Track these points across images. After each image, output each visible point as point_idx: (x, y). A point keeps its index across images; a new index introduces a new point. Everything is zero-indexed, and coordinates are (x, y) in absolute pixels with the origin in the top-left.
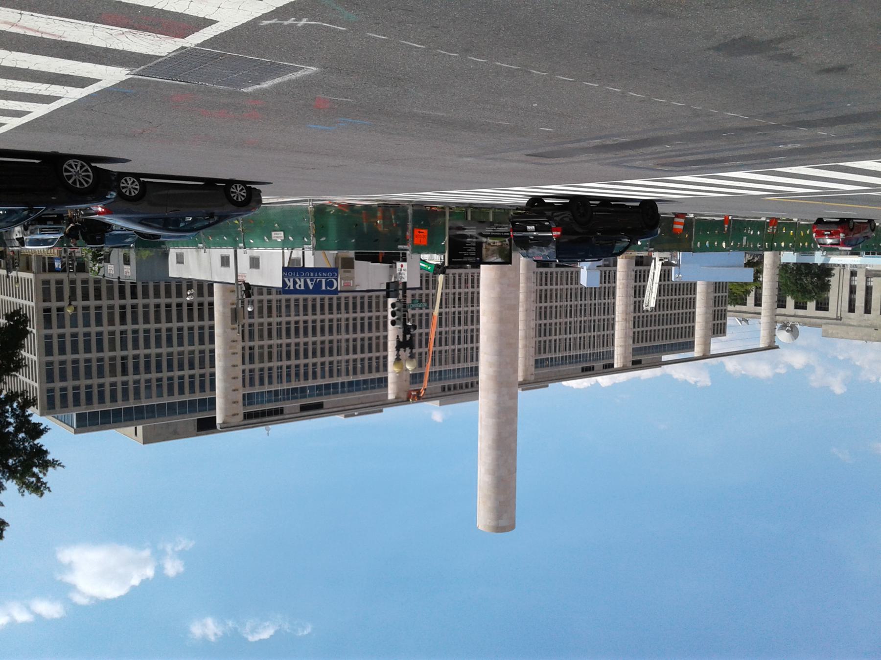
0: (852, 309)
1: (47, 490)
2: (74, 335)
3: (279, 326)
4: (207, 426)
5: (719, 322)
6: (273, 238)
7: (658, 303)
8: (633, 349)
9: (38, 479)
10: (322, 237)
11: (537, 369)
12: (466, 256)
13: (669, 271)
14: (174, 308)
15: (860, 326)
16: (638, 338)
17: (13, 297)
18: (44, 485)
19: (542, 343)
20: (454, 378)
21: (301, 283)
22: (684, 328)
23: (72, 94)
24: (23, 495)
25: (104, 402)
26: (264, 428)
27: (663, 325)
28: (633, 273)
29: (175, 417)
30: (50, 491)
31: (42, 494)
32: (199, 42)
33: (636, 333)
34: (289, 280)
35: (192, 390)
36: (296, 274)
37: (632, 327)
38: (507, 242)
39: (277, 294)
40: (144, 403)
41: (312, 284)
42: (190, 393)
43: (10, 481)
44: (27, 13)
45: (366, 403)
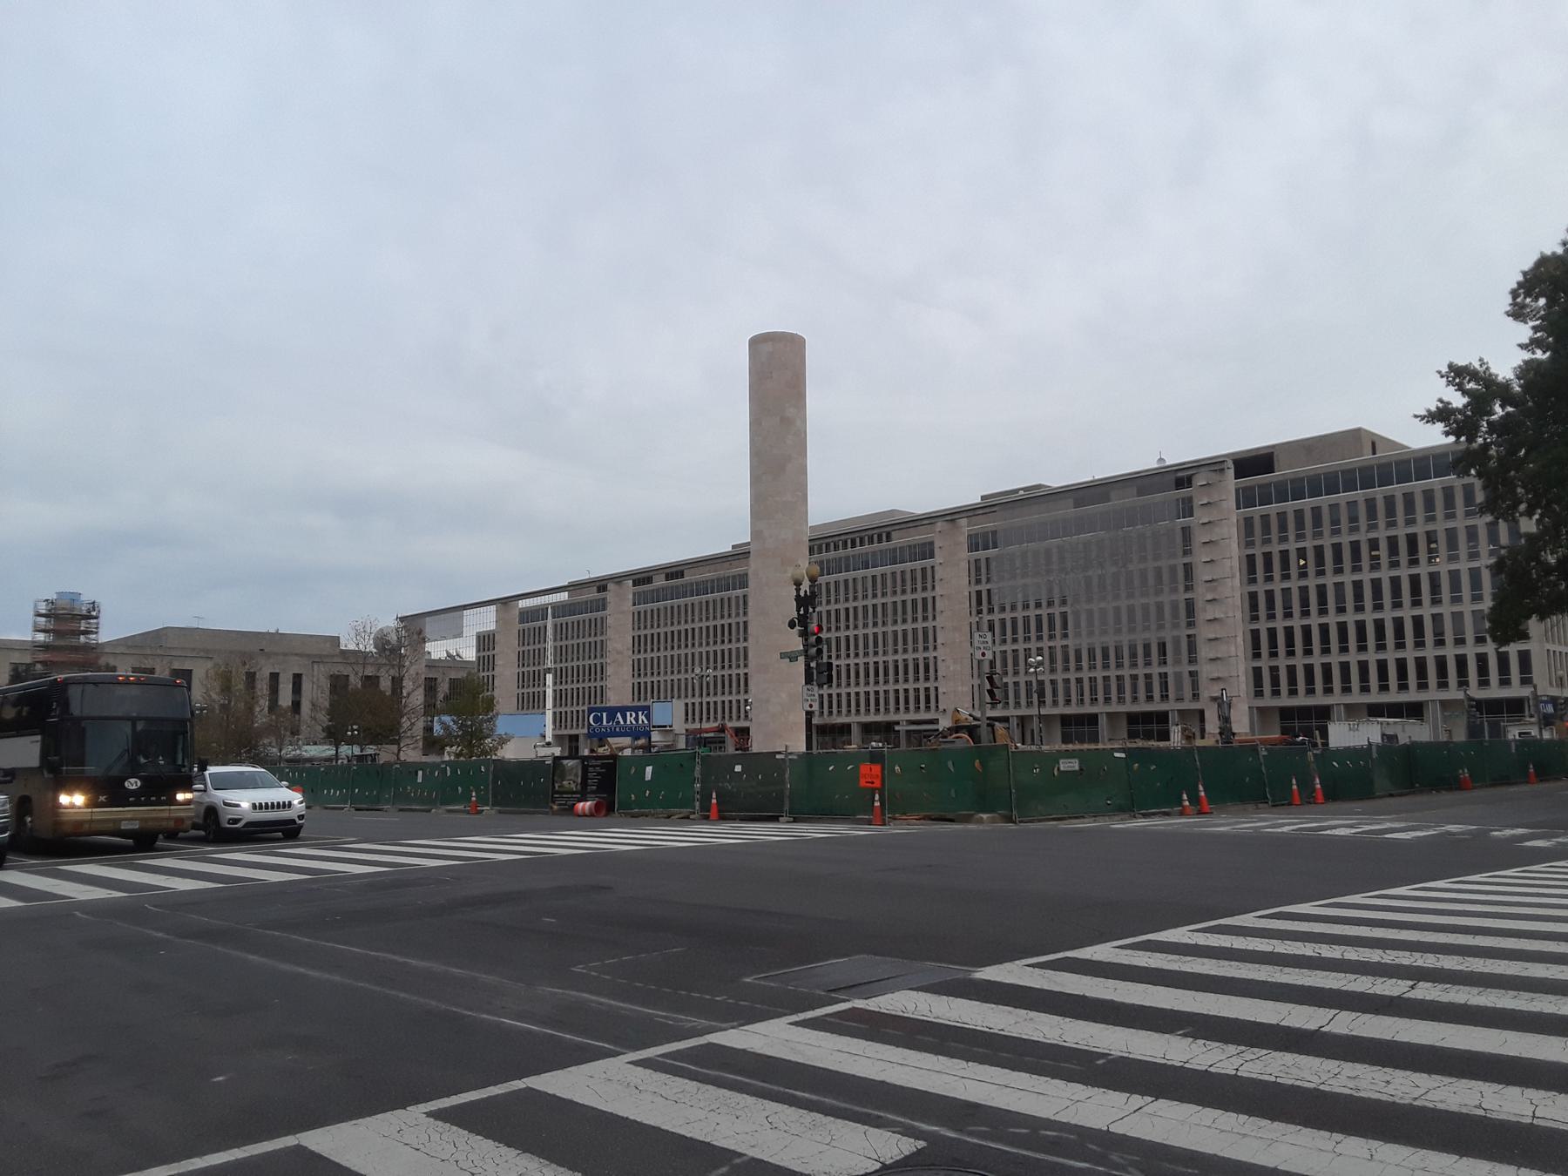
0: (297, 679)
3: (1027, 635)
4: (1253, 464)
5: (486, 653)
6: (1077, 761)
8: (932, 556)
9: (1460, 388)
13: (687, 719)
14: (1449, 637)
15: (285, 655)
16: (701, 610)
18: (1450, 379)
21: (630, 718)
24: (1481, 360)
26: (1168, 463)
29: (1293, 477)
30: (1439, 372)
31: (1451, 366)
34: (643, 722)
38: (557, 785)
40: (1359, 495)
42: (1412, 493)
45: (983, 514)
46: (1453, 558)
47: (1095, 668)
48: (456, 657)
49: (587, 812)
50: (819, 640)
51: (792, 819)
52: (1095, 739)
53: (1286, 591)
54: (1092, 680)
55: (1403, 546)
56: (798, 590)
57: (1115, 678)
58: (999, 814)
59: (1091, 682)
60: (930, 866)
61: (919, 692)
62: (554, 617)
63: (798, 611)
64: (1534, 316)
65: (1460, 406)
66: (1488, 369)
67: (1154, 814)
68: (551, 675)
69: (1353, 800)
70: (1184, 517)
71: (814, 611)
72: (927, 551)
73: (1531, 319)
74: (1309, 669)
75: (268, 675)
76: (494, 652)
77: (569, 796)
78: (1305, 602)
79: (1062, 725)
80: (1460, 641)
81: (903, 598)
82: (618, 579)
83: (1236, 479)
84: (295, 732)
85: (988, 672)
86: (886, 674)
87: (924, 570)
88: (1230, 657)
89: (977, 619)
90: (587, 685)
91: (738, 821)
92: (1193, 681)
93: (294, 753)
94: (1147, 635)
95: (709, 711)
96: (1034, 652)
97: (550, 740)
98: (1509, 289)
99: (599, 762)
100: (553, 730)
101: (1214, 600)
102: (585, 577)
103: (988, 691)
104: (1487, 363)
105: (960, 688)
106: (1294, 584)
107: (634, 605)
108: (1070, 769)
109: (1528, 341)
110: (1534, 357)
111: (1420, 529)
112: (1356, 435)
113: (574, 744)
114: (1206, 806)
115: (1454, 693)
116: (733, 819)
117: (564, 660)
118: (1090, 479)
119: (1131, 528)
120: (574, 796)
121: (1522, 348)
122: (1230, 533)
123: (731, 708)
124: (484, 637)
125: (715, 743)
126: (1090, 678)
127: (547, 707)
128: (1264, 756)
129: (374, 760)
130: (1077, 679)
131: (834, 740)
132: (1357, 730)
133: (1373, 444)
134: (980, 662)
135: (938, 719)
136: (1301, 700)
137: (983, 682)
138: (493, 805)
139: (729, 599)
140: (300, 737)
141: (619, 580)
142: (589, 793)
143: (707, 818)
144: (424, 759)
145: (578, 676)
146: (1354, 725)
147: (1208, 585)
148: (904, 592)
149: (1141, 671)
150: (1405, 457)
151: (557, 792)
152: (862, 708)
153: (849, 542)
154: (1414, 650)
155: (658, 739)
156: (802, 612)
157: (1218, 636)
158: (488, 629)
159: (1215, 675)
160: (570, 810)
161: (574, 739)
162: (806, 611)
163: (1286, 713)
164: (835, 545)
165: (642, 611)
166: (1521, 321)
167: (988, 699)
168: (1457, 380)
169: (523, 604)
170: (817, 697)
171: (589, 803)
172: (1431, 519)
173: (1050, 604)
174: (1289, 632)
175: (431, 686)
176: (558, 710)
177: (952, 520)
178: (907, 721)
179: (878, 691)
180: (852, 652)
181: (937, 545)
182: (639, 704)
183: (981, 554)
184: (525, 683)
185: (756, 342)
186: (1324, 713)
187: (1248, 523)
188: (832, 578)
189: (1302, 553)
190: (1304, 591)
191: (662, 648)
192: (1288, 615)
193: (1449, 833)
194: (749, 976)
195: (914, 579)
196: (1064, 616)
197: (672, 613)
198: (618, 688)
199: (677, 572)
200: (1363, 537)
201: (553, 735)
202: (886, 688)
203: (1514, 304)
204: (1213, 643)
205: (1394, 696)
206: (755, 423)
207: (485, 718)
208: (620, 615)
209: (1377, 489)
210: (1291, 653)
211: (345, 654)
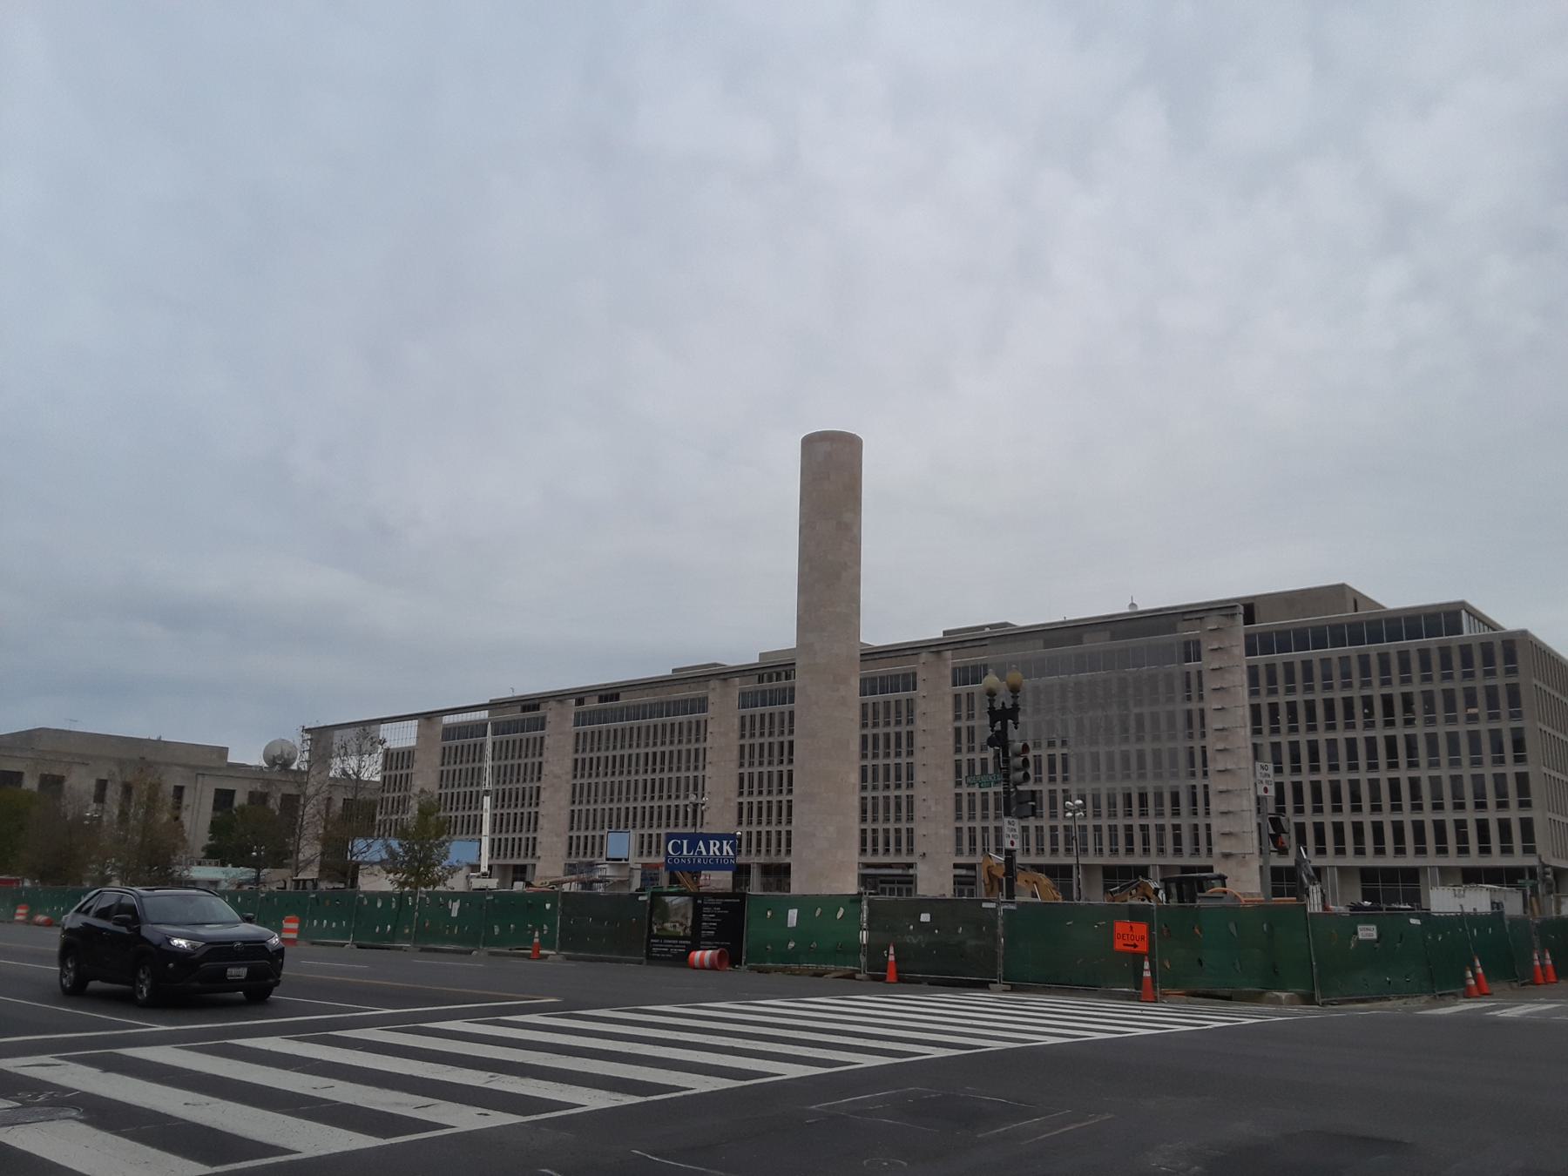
3: (1038, 776)
6: (1375, 927)
8: (704, 710)
10: (1488, 931)
12: (717, 906)
13: (570, 854)
14: (1448, 801)
16: (631, 737)
19: (767, 732)
20: (771, 691)
25: (1440, 649)
26: (1140, 608)
28: (538, 853)
29: (972, 664)
33: (537, 754)
34: (728, 853)
36: (696, 861)
37: (544, 765)
38: (655, 928)
41: (700, 848)
45: (872, 659)
49: (707, 962)
51: (1009, 988)
54: (972, 830)
55: (1320, 712)
56: (991, 701)
57: (1034, 828)
58: (1295, 992)
59: (1037, 831)
63: (992, 726)
68: (489, 798)
70: (891, 692)
77: (674, 942)
79: (1362, 881)
82: (560, 697)
83: (1245, 624)
85: (1274, 812)
86: (769, 814)
87: (698, 723)
88: (1243, 811)
94: (1126, 784)
99: (719, 901)
100: (489, 859)
105: (942, 831)
107: (955, 685)
112: (1342, 588)
115: (1350, 860)
117: (521, 780)
118: (1062, 619)
119: (1135, 669)
120: (681, 942)
124: (398, 754)
125: (893, 882)
127: (483, 833)
130: (995, 827)
131: (780, 881)
132: (1464, 896)
136: (1390, 861)
141: (726, 677)
145: (471, 802)
147: (1218, 733)
149: (1136, 821)
151: (656, 937)
154: (1412, 813)
155: (611, 874)
159: (1227, 830)
160: (682, 960)
162: (1004, 726)
163: (1367, 874)
164: (786, 673)
165: (597, 731)
169: (448, 719)
171: (709, 953)
173: (1051, 744)
176: (497, 836)
177: (725, 679)
180: (657, 795)
181: (920, 677)
182: (676, 831)
186: (1413, 875)
190: (1294, 746)
196: (1065, 757)
199: (612, 695)
200: (1356, 693)
204: (1223, 795)
205: (1496, 860)
207: (436, 842)
209: (1425, 640)
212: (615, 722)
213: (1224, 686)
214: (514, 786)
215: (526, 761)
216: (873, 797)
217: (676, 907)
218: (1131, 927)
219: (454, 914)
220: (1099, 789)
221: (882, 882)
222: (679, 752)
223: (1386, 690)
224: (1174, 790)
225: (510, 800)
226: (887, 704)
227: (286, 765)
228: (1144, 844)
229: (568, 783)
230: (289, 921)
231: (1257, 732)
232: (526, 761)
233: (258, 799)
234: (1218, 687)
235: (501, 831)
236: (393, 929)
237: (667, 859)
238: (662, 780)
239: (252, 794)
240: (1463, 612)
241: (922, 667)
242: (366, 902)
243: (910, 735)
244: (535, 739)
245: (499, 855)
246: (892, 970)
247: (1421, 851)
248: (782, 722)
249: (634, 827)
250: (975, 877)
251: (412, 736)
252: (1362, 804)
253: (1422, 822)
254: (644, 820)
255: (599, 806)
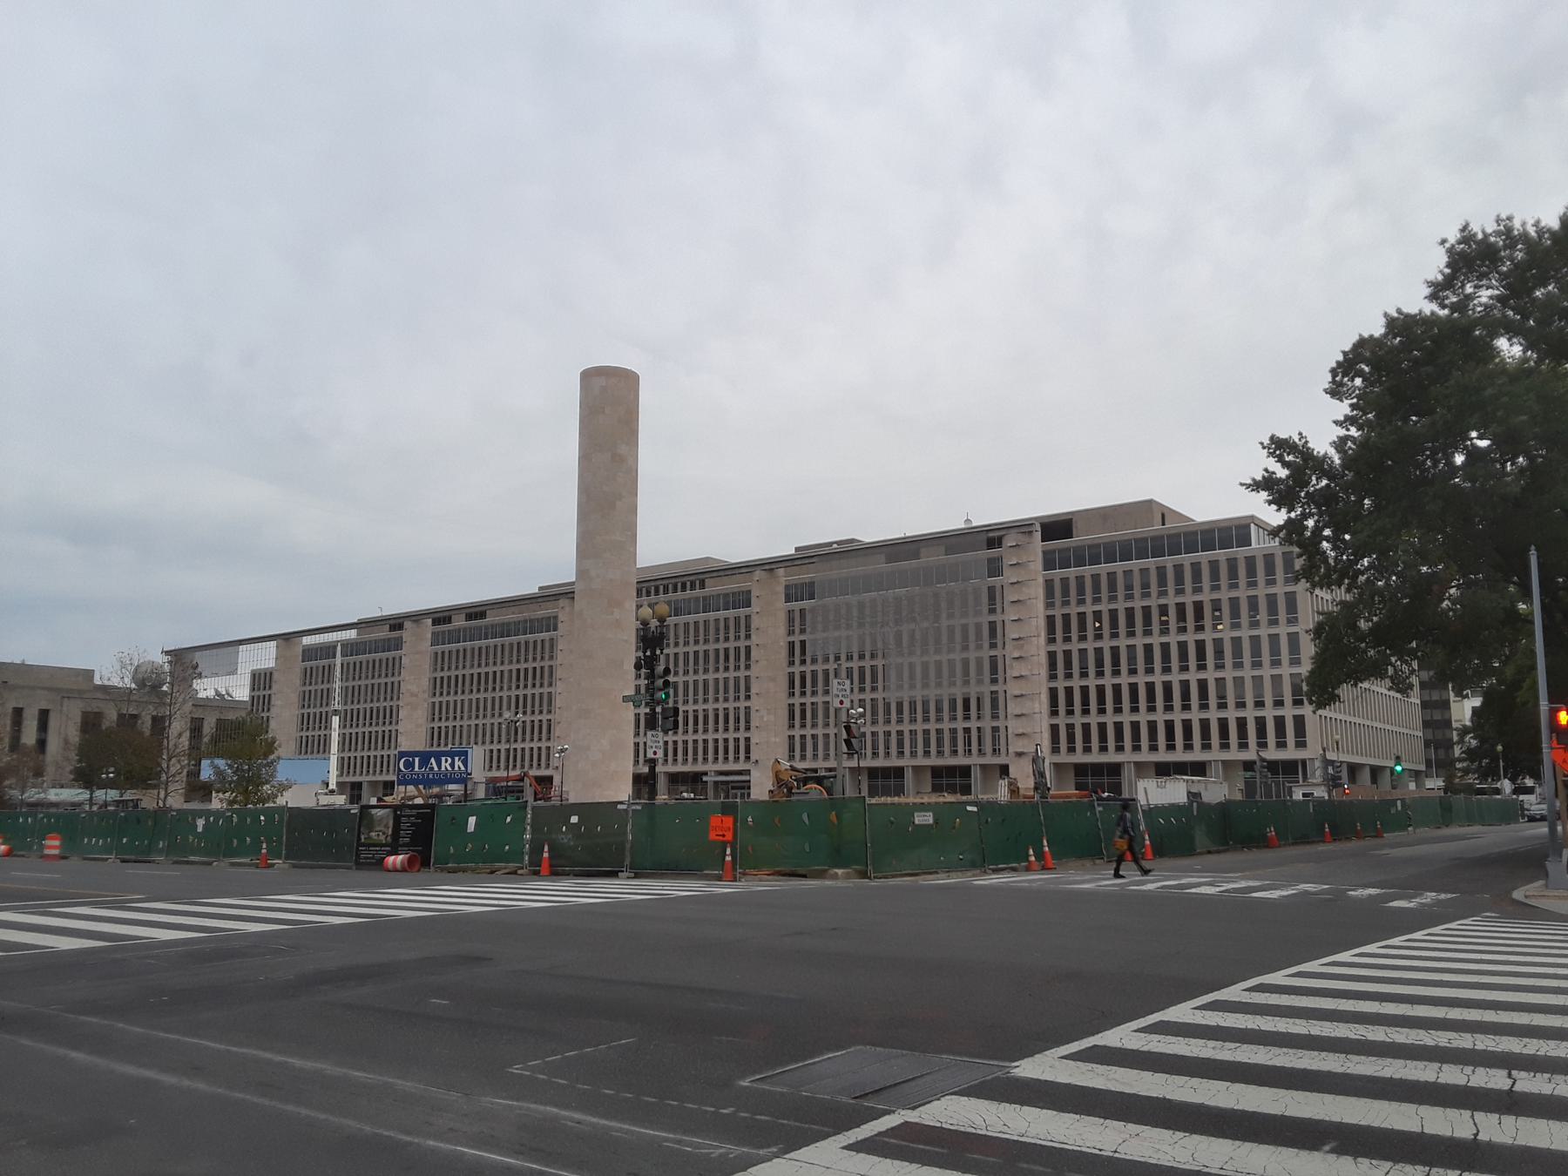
0: (44, 716)
1: (1265, 444)
2: (1220, 667)
4: (1057, 528)
5: (262, 693)
6: (931, 814)
7: (328, 724)
8: (555, 629)
9: (1280, 460)
11: (554, 615)
12: (412, 816)
14: (1231, 701)
15: (33, 688)
16: (473, 657)
17: (1355, 716)
18: (1271, 451)
22: (351, 678)
23: (1114, 1038)
24: (1300, 434)
26: (974, 524)
27: (495, 672)
29: (1089, 542)
30: (1262, 443)
31: (1272, 438)
32: (887, 1117)
34: (459, 768)
35: (1214, 565)
36: (428, 776)
38: (363, 837)
39: (916, 730)
40: (1150, 562)
43: (1322, 453)
44: (1213, 1171)
46: (1255, 624)
47: (915, 721)
48: (226, 696)
50: (666, 684)
51: (633, 875)
52: (900, 791)
53: (1131, 648)
55: (1263, 605)
57: (870, 734)
59: (911, 734)
60: (834, 929)
61: (687, 744)
62: (342, 656)
64: (1350, 395)
65: (1284, 476)
66: (1307, 442)
67: (1003, 869)
68: (338, 718)
69: (1184, 856)
71: (662, 653)
72: (744, 599)
73: (1346, 398)
74: (1205, 724)
75: (10, 711)
76: (400, 678)
78: (1100, 663)
79: (869, 778)
80: (1241, 705)
81: (726, 645)
82: (416, 617)
83: (1042, 542)
84: (39, 772)
88: (1035, 713)
89: (836, 667)
90: (317, 733)
91: (571, 877)
92: (814, 743)
93: (37, 796)
95: (511, 758)
96: (856, 703)
97: (334, 787)
98: (1329, 368)
99: (414, 812)
101: (1021, 657)
102: (376, 614)
103: (845, 740)
104: (1306, 437)
105: (773, 739)
106: (1090, 645)
107: (303, 662)
108: (924, 823)
109: (1342, 419)
110: (1347, 433)
111: (1206, 597)
112: (1149, 504)
113: (356, 793)
114: (1051, 862)
115: (1235, 754)
116: (566, 874)
121: (1337, 425)
122: (1036, 593)
123: (539, 755)
126: (911, 731)
128: (1099, 812)
129: (136, 806)
130: (937, 730)
133: (1163, 516)
134: (837, 710)
135: (749, 770)
136: (1095, 757)
137: (840, 731)
138: (287, 858)
139: (502, 645)
140: (45, 779)
142: (401, 846)
143: (536, 873)
144: (186, 806)
145: (371, 719)
146: (1161, 782)
147: (1015, 643)
148: (727, 639)
150: (1191, 529)
152: (731, 756)
153: (679, 585)
156: (648, 653)
157: (1024, 693)
158: (266, 667)
159: (1020, 731)
160: (379, 864)
161: (357, 787)
162: (653, 653)
163: (1080, 770)
164: (664, 586)
166: (1338, 399)
167: (845, 749)
168: (1278, 452)
170: (661, 744)
171: (401, 857)
172: (1216, 588)
173: (861, 657)
174: (1117, 689)
175: (196, 728)
178: (715, 771)
179: (697, 740)
183: (796, 605)
184: (310, 726)
185: (588, 376)
186: (1115, 769)
187: (1049, 585)
188: (682, 619)
189: (1097, 616)
191: (529, 685)
192: (1133, 672)
193: (1306, 893)
194: (743, 1077)
195: (727, 628)
197: (374, 667)
198: (412, 732)
201: (337, 783)
202: (695, 737)
203: (1334, 381)
204: (1019, 699)
205: (1179, 756)
206: (585, 458)
207: (265, 762)
208: (417, 653)
209: (1058, 571)
210: (1086, 712)
211: (105, 689)
212: (438, 645)
213: (1021, 599)
214: (382, 704)
215: (392, 679)
216: (872, 699)
217: (379, 818)
218: (722, 821)
219: (200, 829)
220: (969, 693)
221: (733, 788)
222: (542, 668)
223: (1180, 600)
224: (966, 696)
225: (378, 718)
226: (687, 625)
227: (156, 687)
228: (814, 751)
229: (425, 700)
230: (52, 839)
231: (1051, 640)
232: (392, 679)
233: (128, 721)
234: (1015, 600)
235: (370, 749)
236: (150, 844)
237: (398, 775)
238: (525, 696)
239: (121, 716)
240: (1252, 525)
241: (756, 585)
242: (235, 819)
243: (748, 649)
244: (511, 645)
245: (382, 771)
246: (545, 864)
247: (1206, 746)
248: (717, 630)
249: (476, 743)
250: (749, 781)
251: (271, 657)
252: (1123, 706)
253: (1283, 717)
254: (364, 743)
255: (465, 723)
